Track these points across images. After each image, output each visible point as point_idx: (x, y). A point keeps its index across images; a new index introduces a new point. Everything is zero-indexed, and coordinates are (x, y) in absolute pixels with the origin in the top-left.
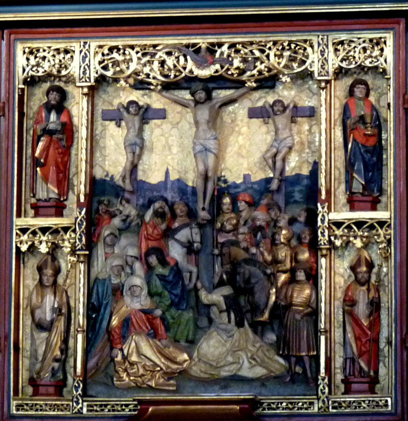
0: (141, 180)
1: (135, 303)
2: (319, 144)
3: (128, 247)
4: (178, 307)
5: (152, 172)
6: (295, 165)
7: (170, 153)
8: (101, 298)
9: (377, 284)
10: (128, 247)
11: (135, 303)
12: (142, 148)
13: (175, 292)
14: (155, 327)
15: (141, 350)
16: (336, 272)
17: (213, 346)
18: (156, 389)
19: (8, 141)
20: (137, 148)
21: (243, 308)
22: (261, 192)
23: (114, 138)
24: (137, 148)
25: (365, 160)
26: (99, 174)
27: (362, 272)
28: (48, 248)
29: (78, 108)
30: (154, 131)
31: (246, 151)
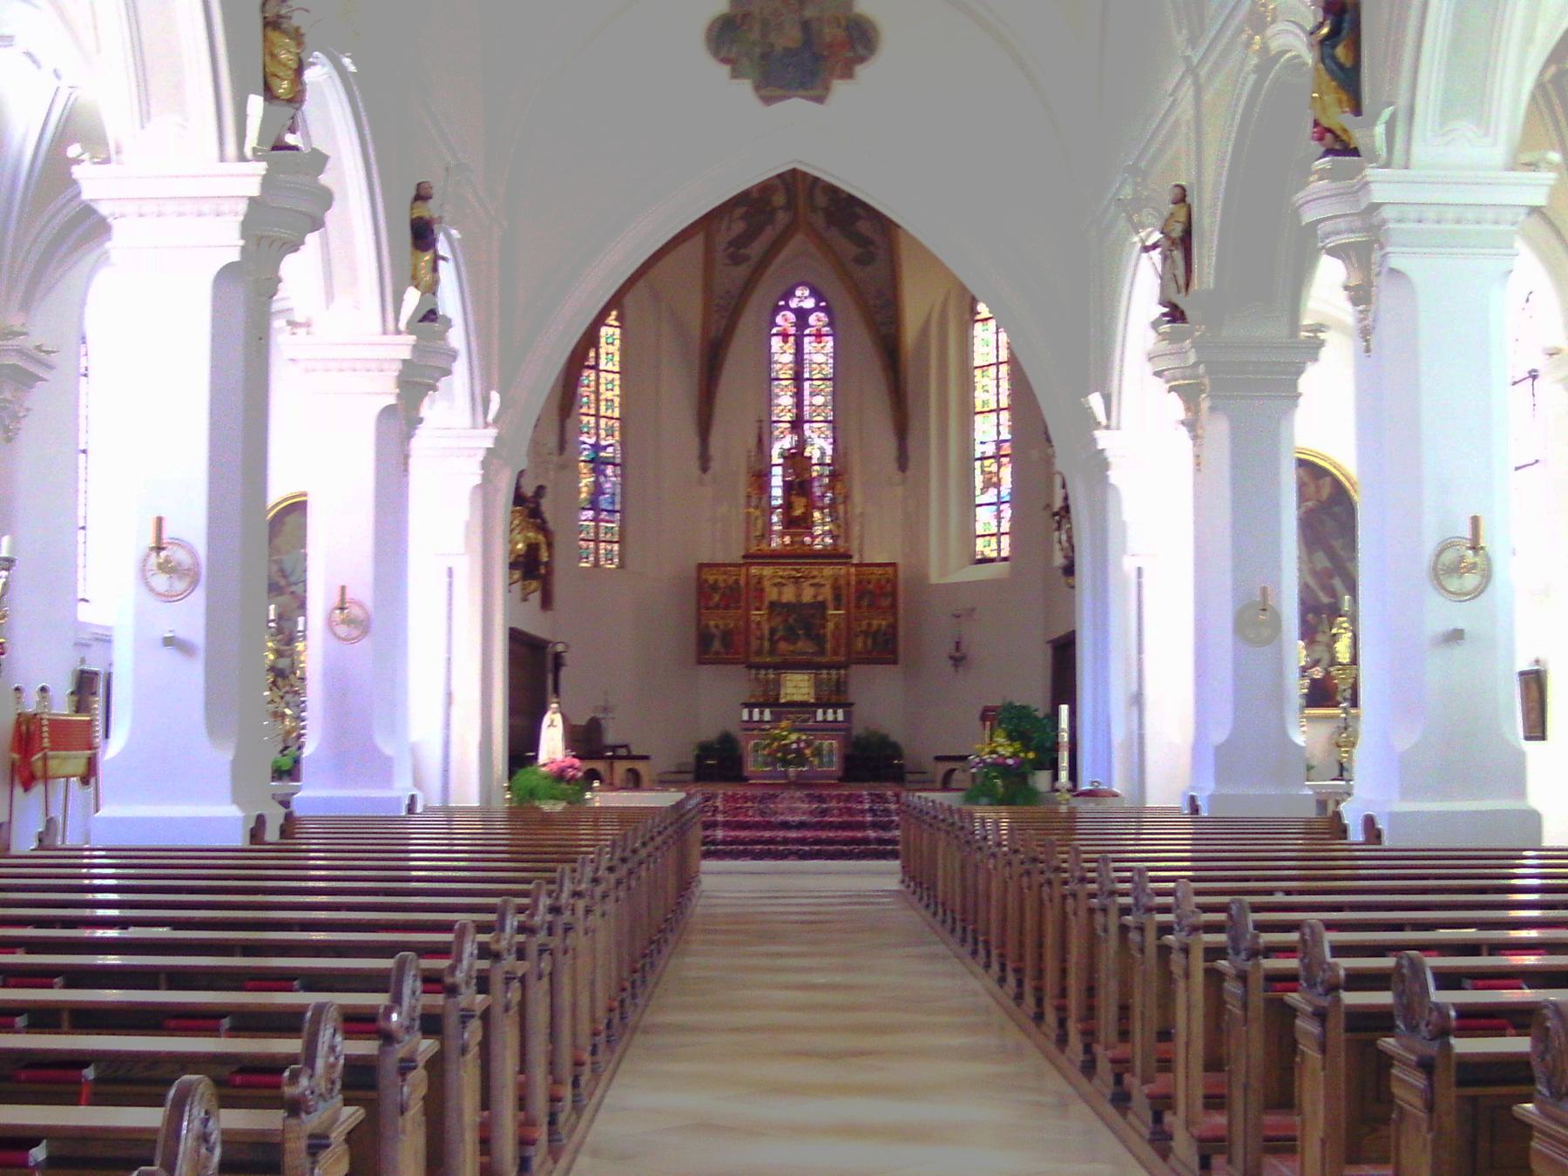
0: (243, 237)
1: (779, 634)
2: (826, 593)
3: (779, 619)
4: (791, 637)
5: (785, 599)
6: (820, 598)
7: (788, 595)
8: (773, 631)
9: (1334, 631)
10: (779, 619)
11: (779, 634)
12: (1337, 137)
13: (791, 630)
14: (783, 638)
15: (783, 645)
16: (830, 626)
17: (800, 644)
18: (1366, 1029)
19: (862, 1053)
20: (780, 594)
21: (808, 636)
22: (811, 605)
23: (775, 590)
24: (780, 594)
25: (837, 597)
27: (837, 626)
28: (191, 576)
29: (767, 584)
30: (785, 589)
31: (808, 595)
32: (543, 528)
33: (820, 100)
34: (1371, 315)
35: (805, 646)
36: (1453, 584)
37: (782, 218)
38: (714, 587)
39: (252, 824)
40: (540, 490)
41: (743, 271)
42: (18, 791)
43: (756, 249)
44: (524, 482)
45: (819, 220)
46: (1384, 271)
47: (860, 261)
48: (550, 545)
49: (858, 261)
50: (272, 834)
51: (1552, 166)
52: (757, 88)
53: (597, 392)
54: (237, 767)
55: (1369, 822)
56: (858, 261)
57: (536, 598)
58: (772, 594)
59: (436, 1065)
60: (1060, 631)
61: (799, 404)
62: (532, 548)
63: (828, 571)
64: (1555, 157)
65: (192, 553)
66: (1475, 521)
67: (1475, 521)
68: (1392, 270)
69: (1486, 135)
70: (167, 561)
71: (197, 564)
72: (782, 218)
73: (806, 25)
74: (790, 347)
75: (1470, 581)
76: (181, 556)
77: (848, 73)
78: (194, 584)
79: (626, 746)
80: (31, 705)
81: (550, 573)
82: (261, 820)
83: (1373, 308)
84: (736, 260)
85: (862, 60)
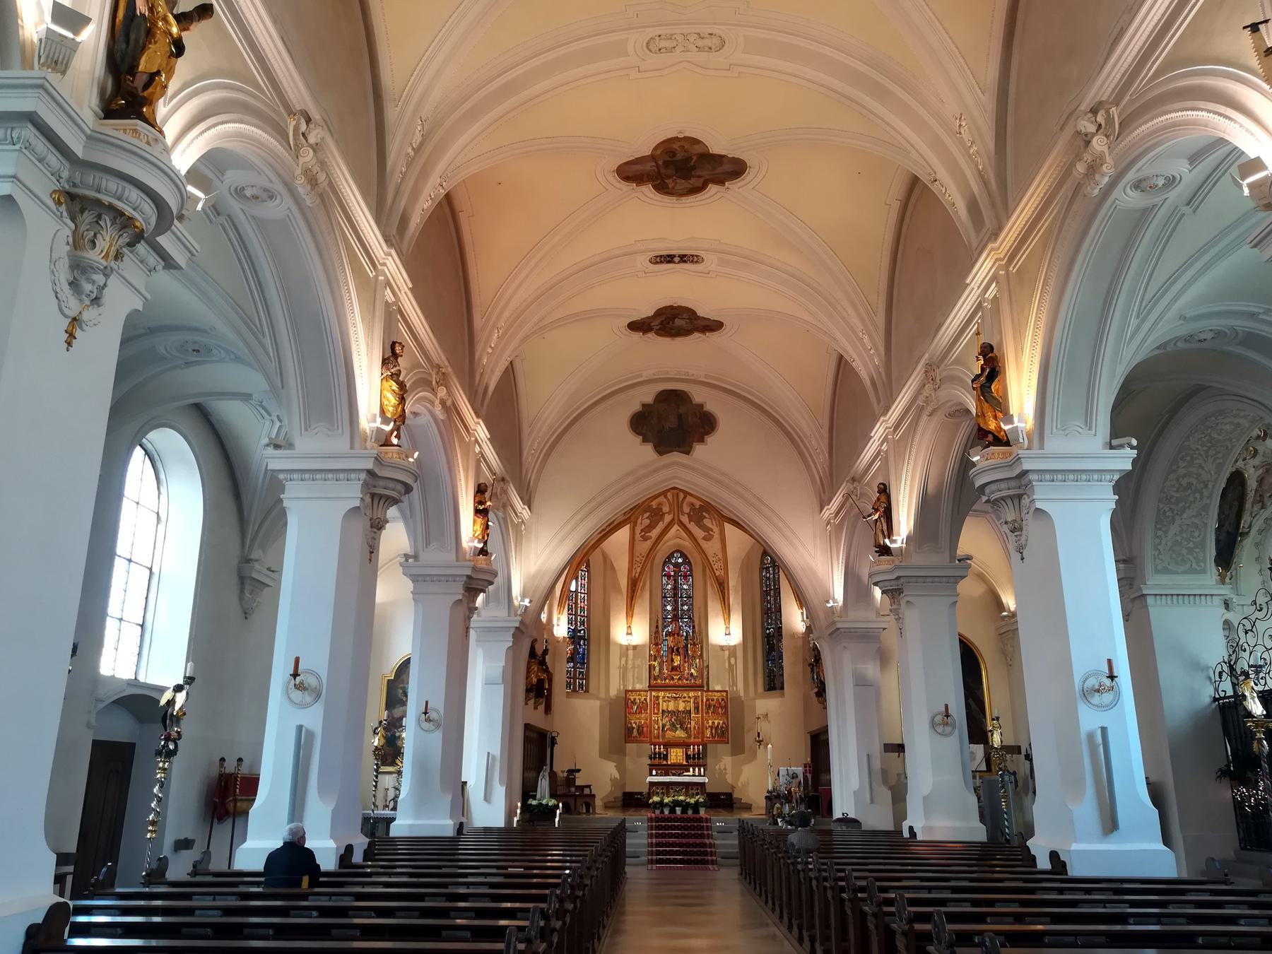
7: (671, 706)
8: (664, 726)
13: (673, 725)
21: (682, 727)
25: (697, 708)
26: (620, 804)
31: (681, 706)
32: (546, 671)
33: (688, 453)
34: (1023, 539)
35: (680, 734)
36: (1096, 699)
37: (668, 518)
38: (634, 702)
39: (342, 852)
40: (546, 652)
41: (649, 544)
42: (215, 821)
43: (655, 533)
44: (537, 647)
45: (685, 519)
46: (1032, 511)
47: (706, 539)
48: (550, 681)
49: (705, 539)
50: (357, 858)
51: (1132, 448)
52: (655, 447)
53: (576, 603)
54: (335, 815)
55: (1054, 856)
56: (705, 539)
57: (542, 707)
58: (663, 706)
59: (967, 149)
60: (814, 727)
61: (675, 609)
62: (541, 682)
63: (691, 694)
64: (1134, 442)
65: (319, 678)
66: (1109, 661)
67: (1109, 661)
68: (1037, 509)
69: (1090, 429)
70: (302, 683)
71: (321, 684)
72: (668, 518)
73: (680, 417)
74: (672, 582)
75: (1107, 698)
76: (312, 681)
77: (701, 440)
78: (318, 696)
79: (589, 786)
80: (230, 767)
81: (550, 694)
82: (349, 849)
83: (1024, 532)
84: (645, 539)
85: (708, 433)
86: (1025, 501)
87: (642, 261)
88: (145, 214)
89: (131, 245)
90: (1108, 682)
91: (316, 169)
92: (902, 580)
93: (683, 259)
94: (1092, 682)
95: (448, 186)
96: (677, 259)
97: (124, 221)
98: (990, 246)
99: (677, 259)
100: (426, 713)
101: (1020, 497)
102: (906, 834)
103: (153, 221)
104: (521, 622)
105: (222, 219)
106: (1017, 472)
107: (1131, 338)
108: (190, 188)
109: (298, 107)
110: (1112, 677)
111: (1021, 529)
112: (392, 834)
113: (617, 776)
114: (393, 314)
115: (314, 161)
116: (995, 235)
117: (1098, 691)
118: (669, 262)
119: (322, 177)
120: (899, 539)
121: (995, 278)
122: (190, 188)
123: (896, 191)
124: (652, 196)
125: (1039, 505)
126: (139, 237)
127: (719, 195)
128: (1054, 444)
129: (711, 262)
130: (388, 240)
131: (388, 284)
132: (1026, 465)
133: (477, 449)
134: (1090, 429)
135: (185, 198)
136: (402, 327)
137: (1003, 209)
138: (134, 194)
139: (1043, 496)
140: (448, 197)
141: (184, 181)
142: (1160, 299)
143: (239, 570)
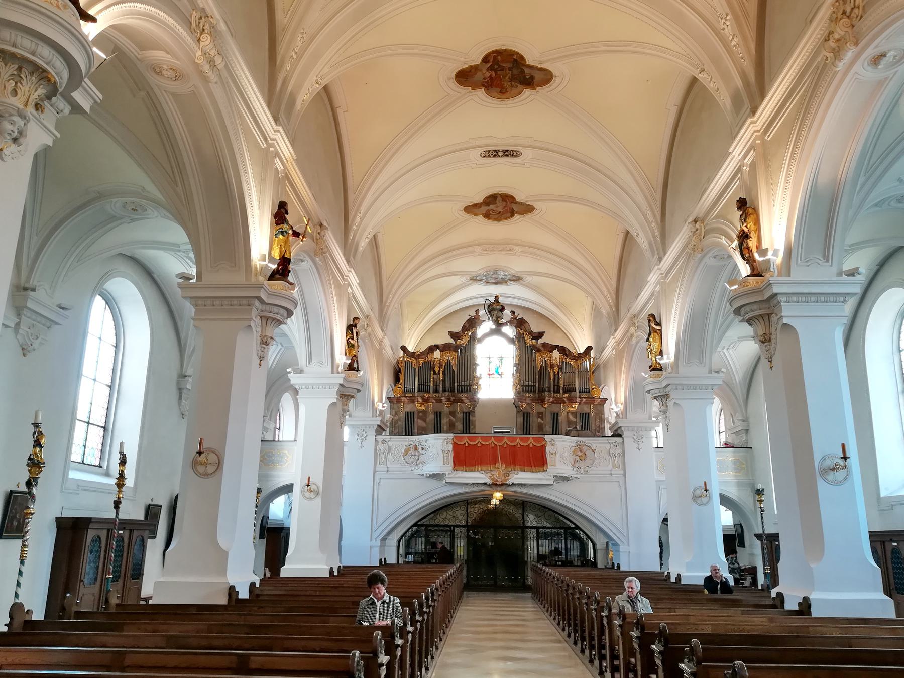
36: (831, 476)
66: (843, 446)
67: (843, 446)
69: (827, 261)
86: (774, 319)
87: (476, 154)
88: (59, 72)
89: (49, 98)
90: (842, 462)
91: (213, 52)
92: (670, 387)
93: (506, 153)
94: (829, 463)
95: (324, 83)
96: (501, 154)
97: (42, 74)
98: (750, 120)
99: (501, 154)
100: (308, 485)
101: (769, 315)
102: (673, 579)
103: (65, 75)
104: (382, 421)
105: (143, 94)
106: (767, 295)
107: (859, 191)
108: (95, 49)
109: (201, 6)
110: (845, 458)
111: (770, 340)
112: (282, 574)
113: (38, 615)
114: (284, 180)
115: (211, 45)
116: (754, 112)
117: (833, 469)
118: (495, 156)
119: (218, 60)
120: (668, 359)
121: (753, 147)
122: (95, 49)
123: (621, 236)
124: (484, 98)
125: (785, 321)
126: (53, 92)
127: (532, 97)
128: (797, 273)
129: (527, 153)
130: (276, 120)
131: (277, 154)
132: (776, 289)
133: (350, 290)
134: (827, 261)
135: (90, 56)
136: (289, 189)
137: (758, 88)
138: (45, 51)
139: (789, 313)
140: (326, 89)
141: (91, 44)
142: (889, 154)
143: (178, 383)
